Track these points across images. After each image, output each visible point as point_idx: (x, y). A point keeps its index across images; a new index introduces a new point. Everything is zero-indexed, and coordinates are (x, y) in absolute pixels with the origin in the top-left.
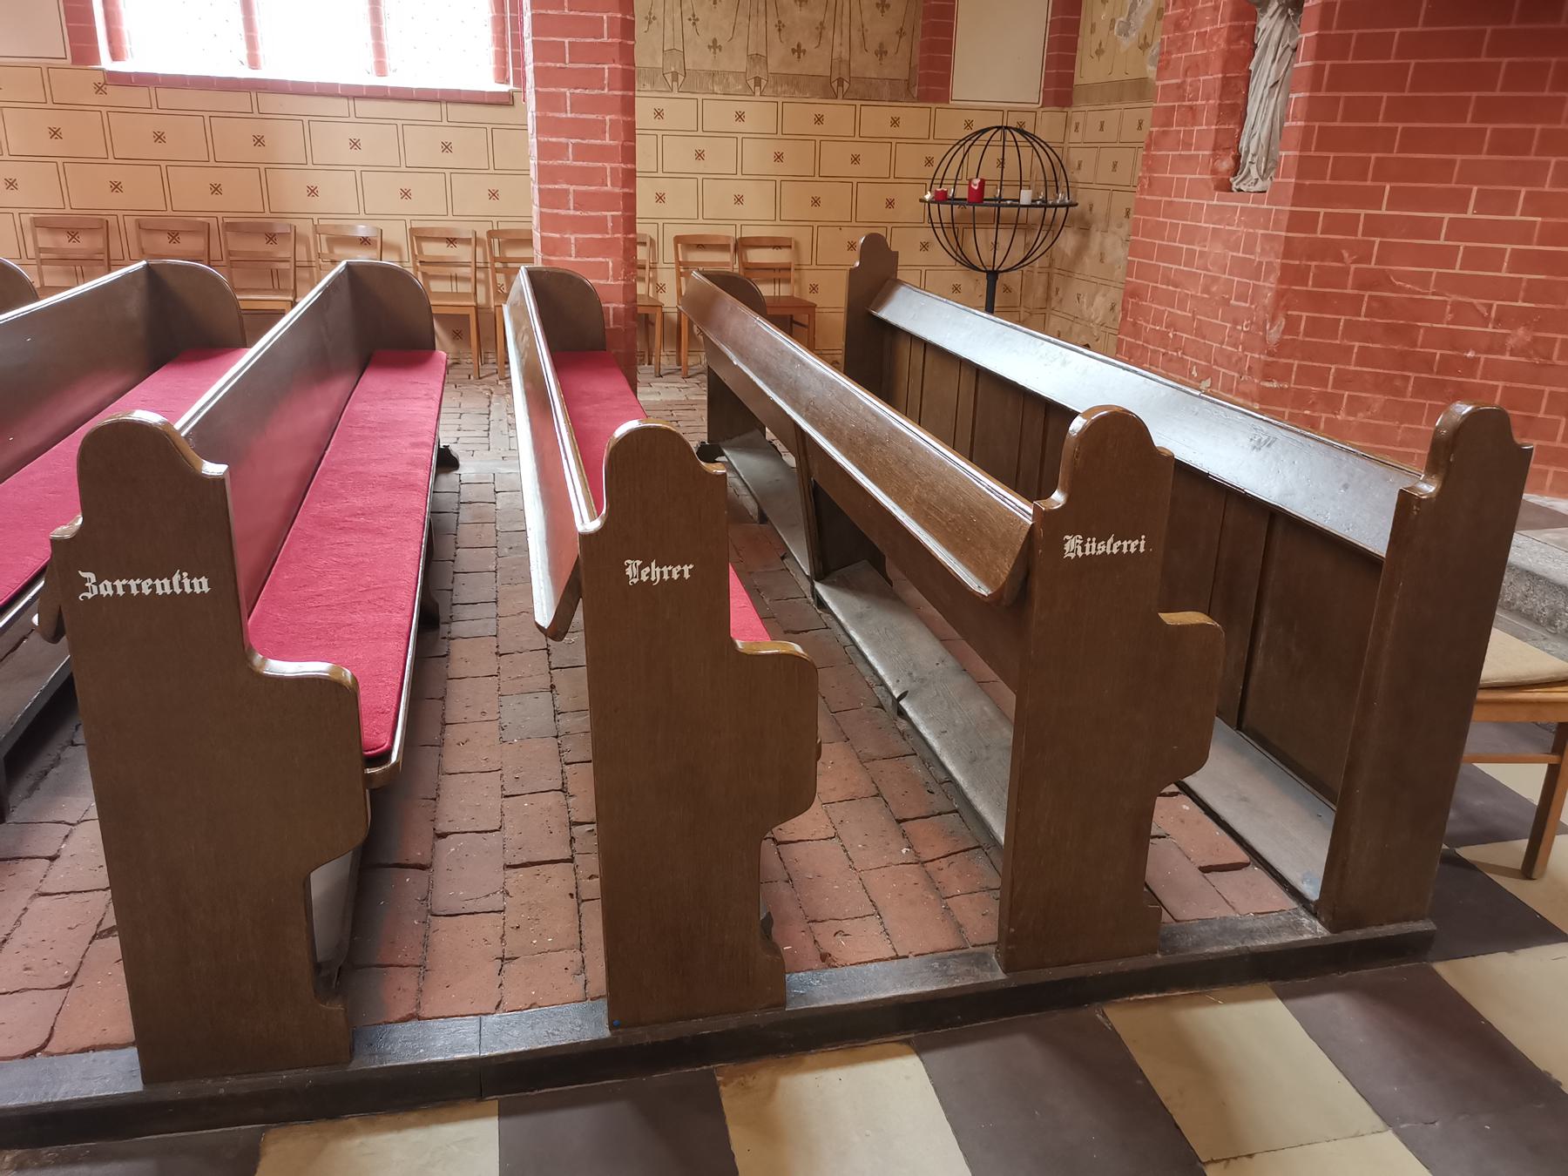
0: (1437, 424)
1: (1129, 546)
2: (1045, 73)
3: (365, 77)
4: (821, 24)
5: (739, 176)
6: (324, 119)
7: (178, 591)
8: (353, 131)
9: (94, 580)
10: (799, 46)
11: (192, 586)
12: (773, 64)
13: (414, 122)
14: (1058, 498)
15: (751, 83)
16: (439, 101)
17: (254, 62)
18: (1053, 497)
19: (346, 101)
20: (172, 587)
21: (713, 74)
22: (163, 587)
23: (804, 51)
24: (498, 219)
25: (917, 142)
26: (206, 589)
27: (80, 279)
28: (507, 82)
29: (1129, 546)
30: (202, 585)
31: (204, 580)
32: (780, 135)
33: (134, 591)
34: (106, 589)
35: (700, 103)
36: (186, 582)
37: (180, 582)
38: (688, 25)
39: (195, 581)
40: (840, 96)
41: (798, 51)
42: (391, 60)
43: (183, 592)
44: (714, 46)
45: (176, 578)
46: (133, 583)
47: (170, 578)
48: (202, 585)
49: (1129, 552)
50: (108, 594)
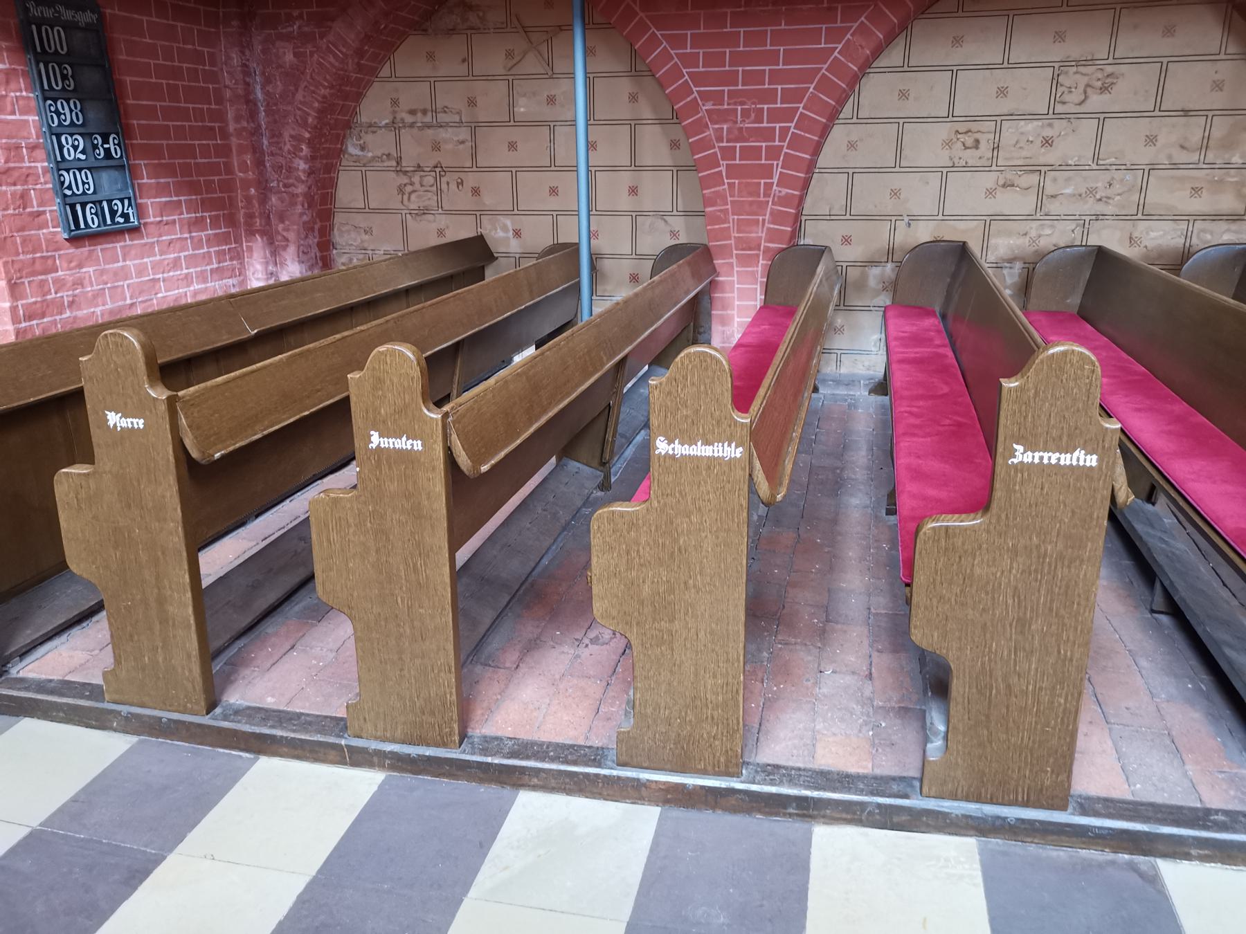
7: (392, 446)
9: (1022, 451)
22: (1066, 459)
27: (28, 328)
30: (1092, 460)
33: (1046, 461)
34: (1028, 458)
35: (471, 73)
39: (1089, 457)
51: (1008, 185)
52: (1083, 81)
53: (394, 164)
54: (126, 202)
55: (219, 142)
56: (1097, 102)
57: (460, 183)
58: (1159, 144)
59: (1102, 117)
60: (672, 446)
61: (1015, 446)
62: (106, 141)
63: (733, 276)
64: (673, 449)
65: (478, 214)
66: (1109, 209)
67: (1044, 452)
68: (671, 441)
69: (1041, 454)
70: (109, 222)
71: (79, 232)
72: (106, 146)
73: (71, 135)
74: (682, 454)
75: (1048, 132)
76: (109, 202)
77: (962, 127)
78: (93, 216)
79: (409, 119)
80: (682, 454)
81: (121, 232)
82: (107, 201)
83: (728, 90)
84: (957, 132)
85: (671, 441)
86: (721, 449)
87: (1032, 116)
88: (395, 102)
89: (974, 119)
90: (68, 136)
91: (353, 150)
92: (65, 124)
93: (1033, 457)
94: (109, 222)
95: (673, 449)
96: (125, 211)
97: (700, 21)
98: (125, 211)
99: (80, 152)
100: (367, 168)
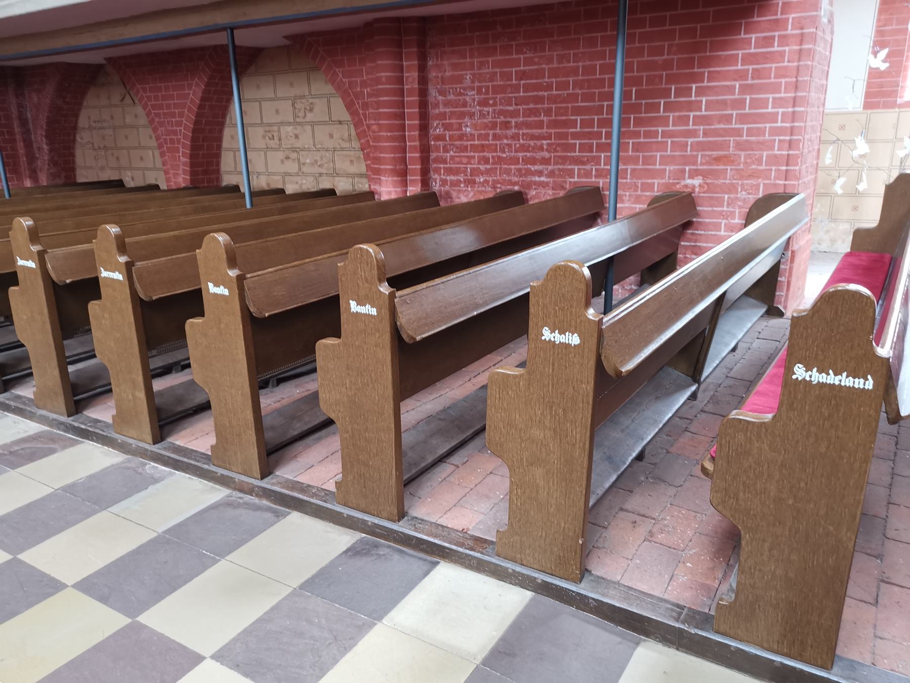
51: (287, 158)
52: (303, 107)
53: (91, 146)
55: (7, 137)
56: (310, 117)
57: (112, 155)
58: (334, 138)
59: (313, 124)
60: (810, 373)
63: (725, 231)
64: (811, 376)
65: (119, 169)
66: (324, 171)
68: (553, 331)
74: (819, 382)
75: (296, 132)
77: (268, 128)
79: (94, 125)
80: (819, 382)
83: (599, 92)
84: (266, 131)
85: (553, 331)
86: (570, 338)
87: (289, 124)
88: (89, 118)
89: (270, 125)
91: (78, 139)
95: (811, 376)
97: (230, 73)
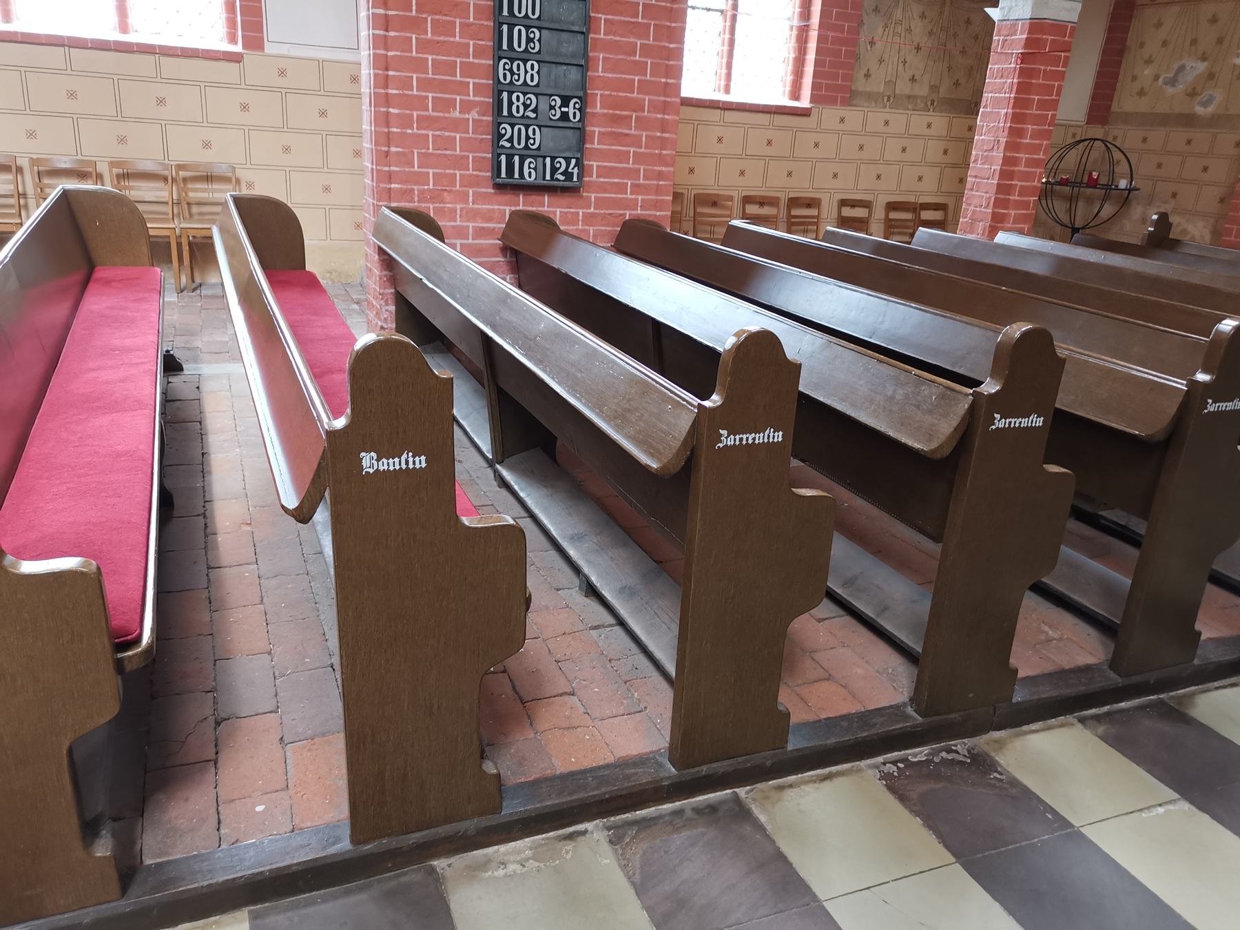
0: (999, 340)
1: (747, 438)
2: (262, 17)
3: (110, 33)
4: (971, 67)
5: (837, 160)
6: (706, 123)
7: (404, 467)
8: (719, 131)
10: (958, 80)
11: (414, 463)
12: (943, 92)
13: (216, 85)
14: (715, 400)
15: (929, 103)
16: (63, 46)
17: (124, 28)
18: (712, 398)
19: (719, 111)
20: (400, 464)
21: (909, 97)
23: (959, 84)
24: (323, 170)
25: (298, 91)
26: (424, 465)
28: (236, 43)
29: (747, 438)
30: (421, 462)
31: (423, 458)
32: (948, 138)
34: (730, 442)
36: (411, 460)
37: (406, 460)
38: (901, 65)
39: (417, 459)
40: (931, 110)
41: (957, 84)
42: (133, 20)
43: (401, 468)
44: (913, 79)
45: (405, 456)
46: (744, 437)
47: (400, 457)
48: (421, 462)
49: (747, 443)
50: (384, 469)
54: (573, 161)
61: (995, 415)
62: (565, 103)
67: (743, 434)
69: (741, 436)
70: (548, 177)
71: (511, 180)
72: (563, 109)
73: (525, 94)
76: (553, 158)
78: (532, 170)
81: (565, 190)
82: (551, 157)
90: (535, 63)
92: (517, 83)
93: (735, 440)
94: (548, 177)
96: (570, 170)
98: (570, 170)
99: (531, 111)
100: (870, 109)
